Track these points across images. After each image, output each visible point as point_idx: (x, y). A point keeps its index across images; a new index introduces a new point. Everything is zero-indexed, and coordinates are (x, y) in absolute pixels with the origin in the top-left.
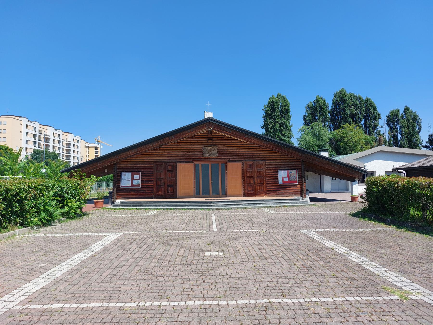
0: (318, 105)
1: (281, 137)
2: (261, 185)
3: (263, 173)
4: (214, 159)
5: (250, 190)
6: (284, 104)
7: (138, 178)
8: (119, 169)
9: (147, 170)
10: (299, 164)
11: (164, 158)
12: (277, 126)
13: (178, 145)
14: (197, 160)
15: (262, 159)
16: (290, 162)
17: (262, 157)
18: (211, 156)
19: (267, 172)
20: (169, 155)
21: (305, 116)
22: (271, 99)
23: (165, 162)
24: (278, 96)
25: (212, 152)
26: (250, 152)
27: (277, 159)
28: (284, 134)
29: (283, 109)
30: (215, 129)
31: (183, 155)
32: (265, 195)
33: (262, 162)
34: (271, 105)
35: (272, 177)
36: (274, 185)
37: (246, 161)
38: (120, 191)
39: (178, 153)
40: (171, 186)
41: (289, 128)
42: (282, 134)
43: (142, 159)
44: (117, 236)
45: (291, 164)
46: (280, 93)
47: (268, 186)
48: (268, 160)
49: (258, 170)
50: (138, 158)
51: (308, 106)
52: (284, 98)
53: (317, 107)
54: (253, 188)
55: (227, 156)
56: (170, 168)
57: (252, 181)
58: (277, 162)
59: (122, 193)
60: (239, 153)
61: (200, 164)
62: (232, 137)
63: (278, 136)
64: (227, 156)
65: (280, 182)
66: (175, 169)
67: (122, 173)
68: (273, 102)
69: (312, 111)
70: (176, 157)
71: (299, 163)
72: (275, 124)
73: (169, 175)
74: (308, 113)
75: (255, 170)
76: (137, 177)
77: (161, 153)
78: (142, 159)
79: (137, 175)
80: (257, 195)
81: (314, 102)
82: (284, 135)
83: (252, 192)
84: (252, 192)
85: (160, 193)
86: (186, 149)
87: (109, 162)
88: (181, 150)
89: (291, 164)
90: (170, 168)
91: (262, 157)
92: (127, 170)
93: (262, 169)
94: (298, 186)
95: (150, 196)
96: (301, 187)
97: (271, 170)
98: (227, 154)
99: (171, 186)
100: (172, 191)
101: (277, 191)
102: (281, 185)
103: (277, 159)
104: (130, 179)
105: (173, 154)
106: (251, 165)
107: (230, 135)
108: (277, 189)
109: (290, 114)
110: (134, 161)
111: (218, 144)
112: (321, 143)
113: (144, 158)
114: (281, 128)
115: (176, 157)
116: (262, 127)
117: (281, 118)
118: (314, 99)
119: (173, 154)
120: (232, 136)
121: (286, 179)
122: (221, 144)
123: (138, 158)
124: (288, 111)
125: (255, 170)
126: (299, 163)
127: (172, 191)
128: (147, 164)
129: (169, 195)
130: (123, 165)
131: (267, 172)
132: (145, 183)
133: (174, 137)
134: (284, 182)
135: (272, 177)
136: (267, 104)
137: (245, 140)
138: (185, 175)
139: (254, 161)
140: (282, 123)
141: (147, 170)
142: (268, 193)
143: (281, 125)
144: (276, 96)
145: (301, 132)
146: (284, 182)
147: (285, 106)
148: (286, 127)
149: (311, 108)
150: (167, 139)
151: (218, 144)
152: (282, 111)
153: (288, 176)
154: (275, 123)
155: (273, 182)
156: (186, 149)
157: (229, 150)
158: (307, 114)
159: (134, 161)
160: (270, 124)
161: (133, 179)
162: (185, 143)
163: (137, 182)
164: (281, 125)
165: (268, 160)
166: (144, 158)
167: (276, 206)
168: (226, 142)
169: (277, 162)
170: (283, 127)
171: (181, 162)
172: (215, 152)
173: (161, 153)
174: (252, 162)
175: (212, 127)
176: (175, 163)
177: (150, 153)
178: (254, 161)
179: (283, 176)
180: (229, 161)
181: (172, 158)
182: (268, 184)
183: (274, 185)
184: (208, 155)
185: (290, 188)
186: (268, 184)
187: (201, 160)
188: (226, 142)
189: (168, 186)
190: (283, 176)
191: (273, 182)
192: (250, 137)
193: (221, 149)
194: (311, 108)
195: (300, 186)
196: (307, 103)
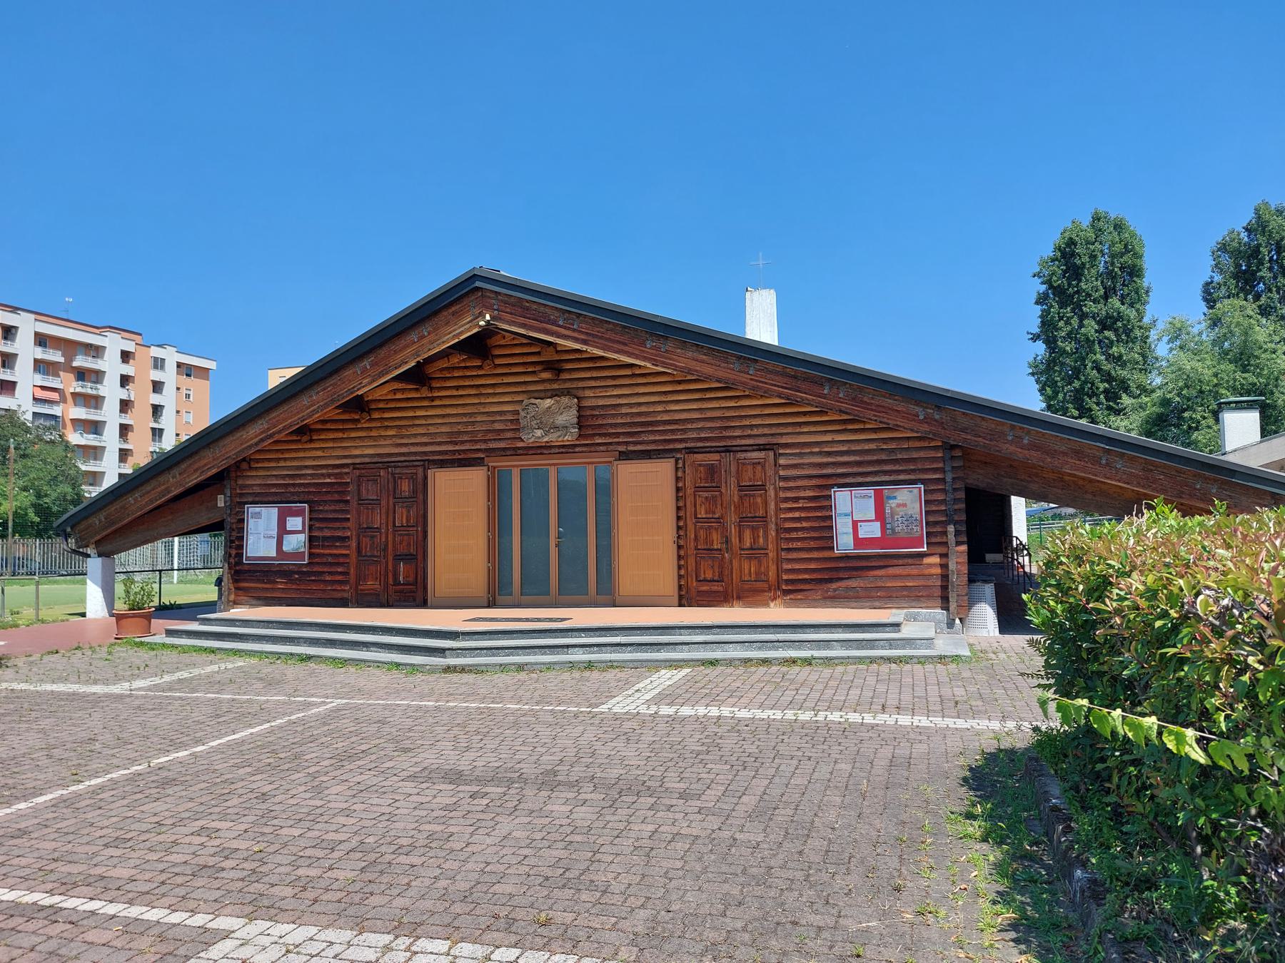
0: (1262, 240)
1: (1107, 367)
2: (756, 553)
3: (766, 503)
4: (566, 449)
5: (709, 576)
6: (1119, 248)
7: (300, 528)
8: (241, 495)
9: (329, 497)
10: (934, 459)
11: (386, 451)
12: (1091, 327)
13: (432, 399)
14: (503, 452)
15: (762, 441)
16: (892, 451)
17: (760, 431)
18: (553, 438)
19: (786, 500)
20: (402, 437)
21: (1207, 284)
22: (1067, 235)
23: (386, 465)
24: (1096, 218)
25: (554, 417)
26: (709, 415)
27: (828, 438)
28: (1121, 356)
29: (1113, 264)
30: (508, 317)
31: (453, 438)
32: (774, 599)
33: (762, 454)
34: (1064, 255)
35: (807, 519)
36: (815, 555)
37: (691, 451)
38: (247, 579)
39: (432, 430)
40: (409, 558)
41: (1138, 333)
42: (1109, 357)
43: (314, 458)
44: (676, 679)
45: (896, 461)
46: (1101, 209)
47: (790, 560)
48: (787, 446)
49: (741, 488)
50: (301, 454)
51: (1223, 247)
52: (1119, 227)
53: (1259, 245)
54: (721, 567)
55: (618, 435)
56: (405, 487)
57: (715, 536)
58: (829, 454)
59: (252, 581)
60: (666, 417)
61: (515, 469)
62: (589, 349)
63: (1097, 367)
64: (618, 435)
65: (844, 542)
66: (421, 492)
67: (252, 509)
68: (1071, 242)
69: (1238, 266)
70: (426, 444)
71: (932, 454)
72: (1081, 321)
73: (401, 517)
74: (1221, 272)
75: (730, 491)
76: (295, 523)
77: (374, 433)
78: (314, 458)
79: (297, 515)
80: (739, 598)
81: (1246, 229)
82: (1118, 359)
83: (716, 587)
84: (716, 587)
85: (371, 584)
86: (460, 411)
87: (196, 471)
88: (443, 416)
89: (896, 461)
90: (405, 487)
91: (760, 431)
92: (264, 499)
93: (762, 487)
94: (927, 560)
95: (339, 595)
96: (944, 566)
97: (804, 488)
98: (616, 425)
99: (409, 558)
100: (411, 579)
101: (831, 580)
102: (847, 557)
103: (828, 438)
104: (275, 533)
105: (415, 435)
106: (712, 471)
107: (576, 340)
108: (835, 575)
109: (1145, 282)
110: (288, 464)
111: (581, 384)
112: (1253, 379)
113: (319, 453)
114: (1107, 333)
115: (426, 444)
116: (1035, 338)
117: (1106, 297)
118: (1248, 217)
119: (415, 435)
120: (585, 342)
121: (872, 530)
122: (593, 384)
123: (301, 454)
124: (1134, 272)
125: (730, 491)
126: (932, 454)
127: (411, 579)
128: (329, 476)
129: (401, 592)
130: (254, 480)
131: (786, 500)
132: (323, 547)
133: (372, 365)
134: (859, 542)
135: (807, 519)
136: (1049, 252)
137: (645, 359)
138: (458, 508)
139: (727, 450)
140: (1108, 316)
141: (329, 497)
142: (786, 592)
143: (1106, 323)
144: (1086, 222)
145: (1170, 341)
146: (859, 542)
147: (1122, 254)
148: (1128, 332)
149: (1236, 254)
150: (348, 373)
151: (581, 384)
152: (1110, 274)
153: (880, 515)
154: (1083, 316)
155: (812, 545)
156: (460, 411)
157: (624, 410)
158: (1218, 278)
159: (288, 464)
160: (1061, 324)
161: (283, 531)
162: (457, 388)
163: (297, 542)
164: (1106, 323)
165: (787, 446)
166: (319, 453)
167: (746, 661)
168: (614, 378)
169: (829, 454)
170: (1116, 330)
171: (442, 464)
172: (568, 417)
173: (374, 433)
174: (717, 456)
175: (490, 308)
176: (420, 470)
177: (340, 435)
178: (727, 450)
179: (853, 515)
180: (625, 456)
181: (413, 449)
182: (789, 550)
183: (815, 555)
184: (539, 433)
185: (891, 571)
186: (789, 550)
187: (515, 452)
188: (614, 378)
189: (398, 558)
190: (853, 515)
191: (812, 545)
192: (670, 345)
193: (593, 408)
194: (1236, 254)
195: (935, 560)
196: (1219, 235)
